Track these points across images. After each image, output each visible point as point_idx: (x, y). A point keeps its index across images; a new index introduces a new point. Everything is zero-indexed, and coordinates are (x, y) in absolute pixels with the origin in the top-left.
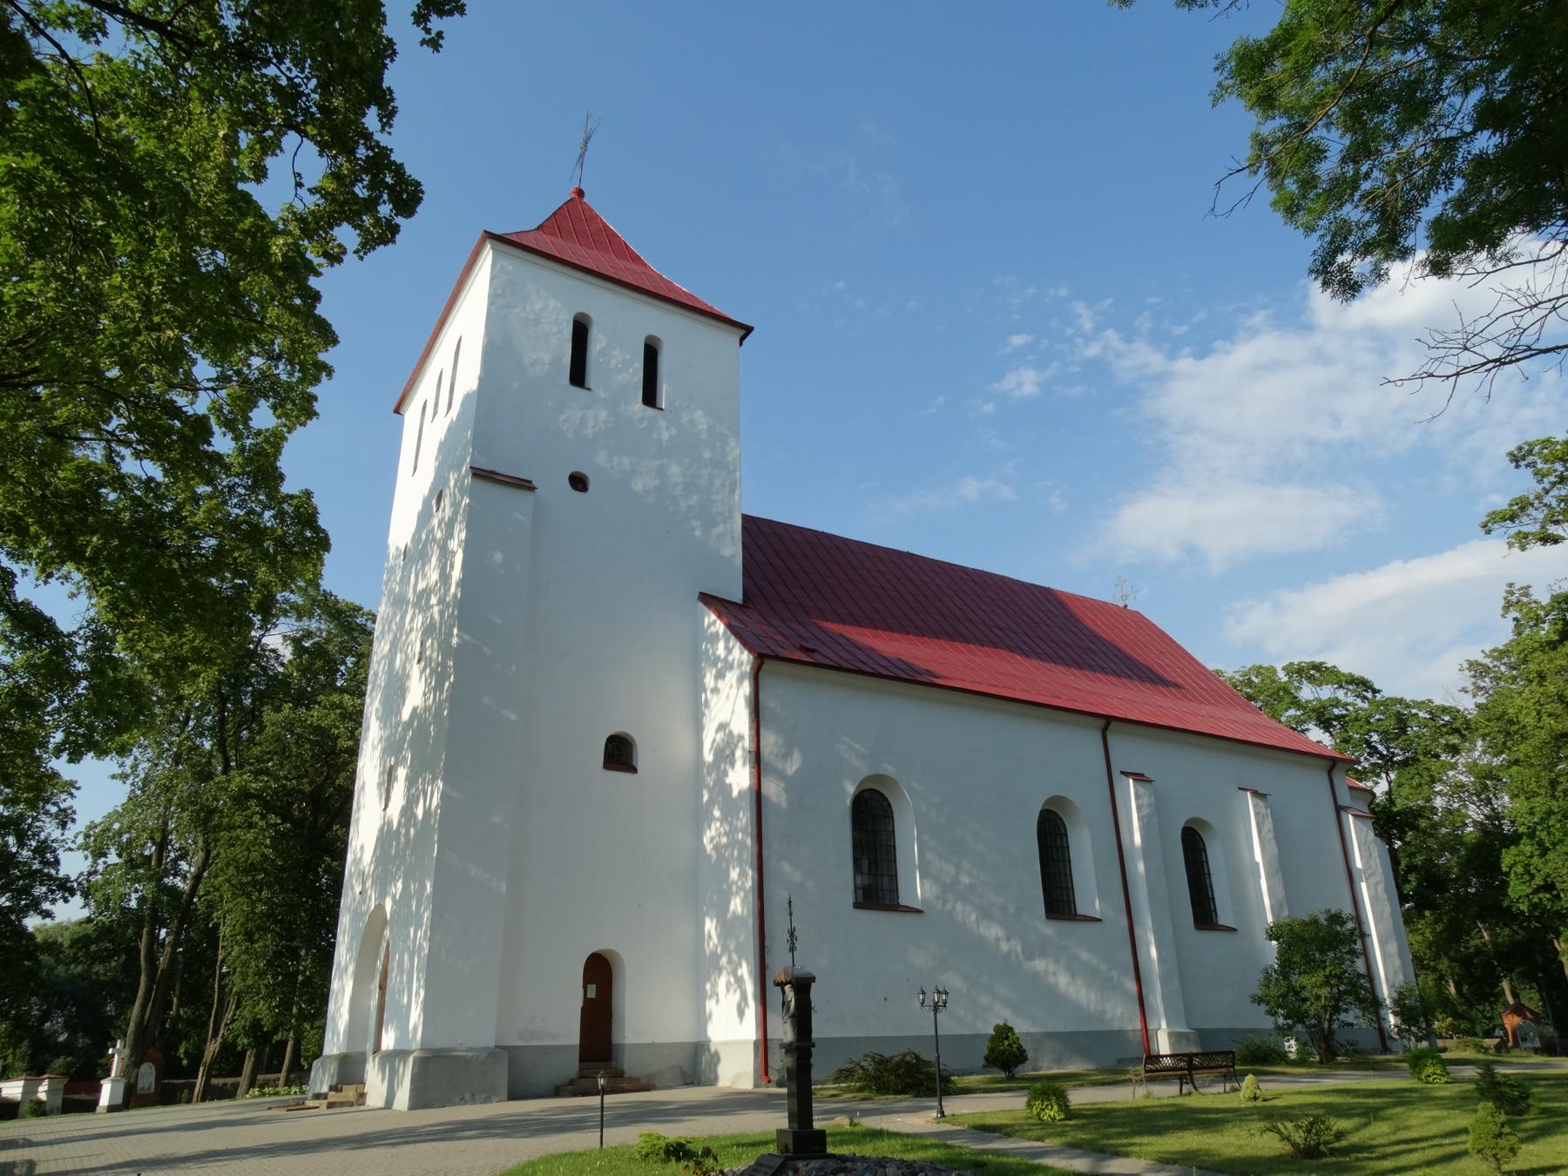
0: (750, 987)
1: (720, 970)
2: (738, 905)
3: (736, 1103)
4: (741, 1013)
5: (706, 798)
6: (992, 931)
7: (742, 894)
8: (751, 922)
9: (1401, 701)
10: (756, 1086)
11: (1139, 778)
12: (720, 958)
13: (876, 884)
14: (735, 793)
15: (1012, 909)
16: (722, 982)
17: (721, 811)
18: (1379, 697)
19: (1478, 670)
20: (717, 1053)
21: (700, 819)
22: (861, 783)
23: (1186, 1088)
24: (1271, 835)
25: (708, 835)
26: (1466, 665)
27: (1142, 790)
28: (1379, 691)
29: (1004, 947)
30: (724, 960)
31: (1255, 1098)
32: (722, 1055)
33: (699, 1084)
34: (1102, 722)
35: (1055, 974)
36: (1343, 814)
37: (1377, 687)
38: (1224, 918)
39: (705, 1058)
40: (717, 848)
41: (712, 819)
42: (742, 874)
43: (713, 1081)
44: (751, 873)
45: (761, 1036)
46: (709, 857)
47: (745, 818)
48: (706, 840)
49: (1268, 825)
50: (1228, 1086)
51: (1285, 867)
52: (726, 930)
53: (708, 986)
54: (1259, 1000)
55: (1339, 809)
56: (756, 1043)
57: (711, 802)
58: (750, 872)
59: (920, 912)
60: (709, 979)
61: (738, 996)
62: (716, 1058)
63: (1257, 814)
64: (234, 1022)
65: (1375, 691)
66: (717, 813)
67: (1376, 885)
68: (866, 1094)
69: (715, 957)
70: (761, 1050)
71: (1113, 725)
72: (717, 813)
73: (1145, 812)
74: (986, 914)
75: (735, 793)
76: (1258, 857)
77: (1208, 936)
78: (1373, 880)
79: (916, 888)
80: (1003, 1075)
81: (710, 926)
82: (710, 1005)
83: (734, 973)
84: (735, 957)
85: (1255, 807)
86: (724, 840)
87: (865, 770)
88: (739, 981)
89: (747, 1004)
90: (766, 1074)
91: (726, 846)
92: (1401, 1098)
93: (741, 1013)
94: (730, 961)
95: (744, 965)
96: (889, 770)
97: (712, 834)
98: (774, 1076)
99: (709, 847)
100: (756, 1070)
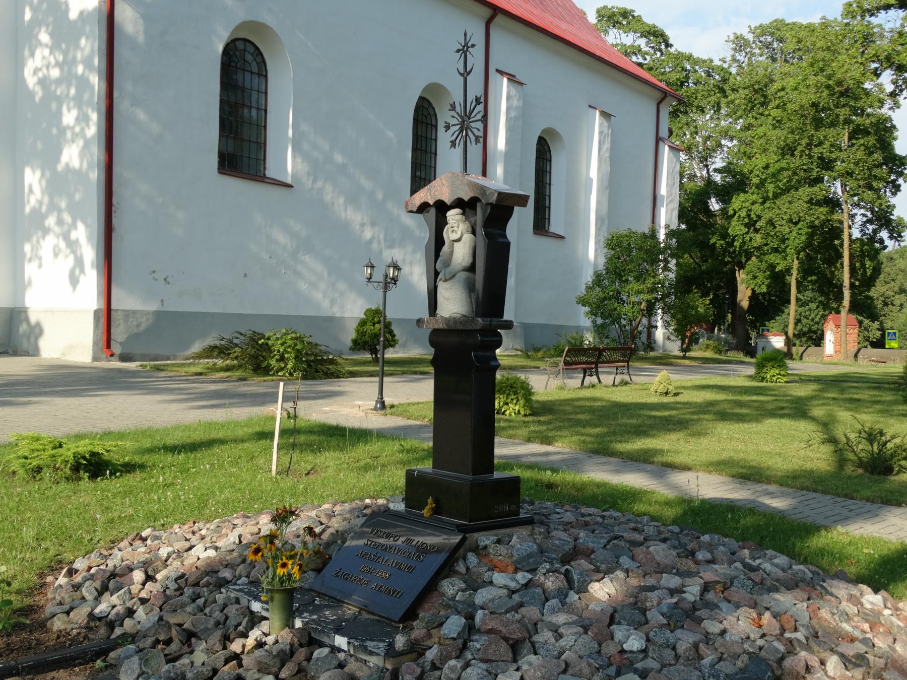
0: (90, 253)
1: (46, 231)
2: (78, 154)
3: (67, 381)
4: (74, 281)
5: (28, 15)
6: (355, 217)
7: (81, 143)
8: (95, 176)
9: (689, 58)
10: (95, 359)
11: (512, 79)
12: (45, 217)
13: (241, 150)
14: (73, 15)
15: (380, 196)
16: (49, 242)
17: (52, 35)
18: (672, 50)
19: (740, 44)
20: (38, 325)
21: (20, 42)
22: (237, 29)
23: (588, 380)
24: (607, 155)
25: (30, 66)
26: (732, 38)
27: (513, 92)
28: (671, 46)
29: (368, 234)
30: (51, 221)
31: (667, 393)
32: (46, 326)
33: (15, 353)
34: (487, 12)
35: (411, 264)
36: (661, 143)
37: (671, 42)
38: (555, 226)
39: (23, 328)
40: (43, 82)
41: (34, 44)
42: (83, 119)
43: (34, 352)
44: (95, 117)
45: (103, 306)
46: (32, 94)
47: (89, 46)
48: (28, 72)
49: (607, 145)
50: (619, 378)
51: (613, 185)
52: (58, 183)
53: (27, 248)
54: (583, 301)
55: (658, 140)
56: (96, 313)
57: (36, 23)
58: (94, 116)
59: (291, 186)
60: (29, 239)
61: (71, 261)
62: (37, 331)
63: (601, 133)
64: (858, 594)
65: (668, 45)
66: (44, 37)
67: (672, 210)
68: (238, 373)
69: (38, 217)
70: (103, 320)
71: (500, 19)
72: (44, 37)
73: (513, 114)
74: (353, 199)
75: (73, 15)
76: (594, 173)
77: (543, 242)
78: (671, 206)
79: (285, 161)
80: (368, 356)
81: (32, 178)
82: (30, 270)
83: (66, 237)
84: (67, 218)
85: (600, 125)
86: (55, 73)
87: (241, 16)
88: (72, 245)
89: (82, 271)
90: (108, 346)
91: (58, 81)
92: (190, 364)
93: (74, 281)
94: (60, 222)
95: (81, 226)
96: (267, 18)
97: (39, 64)
98: (116, 349)
99: (31, 81)
100: (95, 343)
